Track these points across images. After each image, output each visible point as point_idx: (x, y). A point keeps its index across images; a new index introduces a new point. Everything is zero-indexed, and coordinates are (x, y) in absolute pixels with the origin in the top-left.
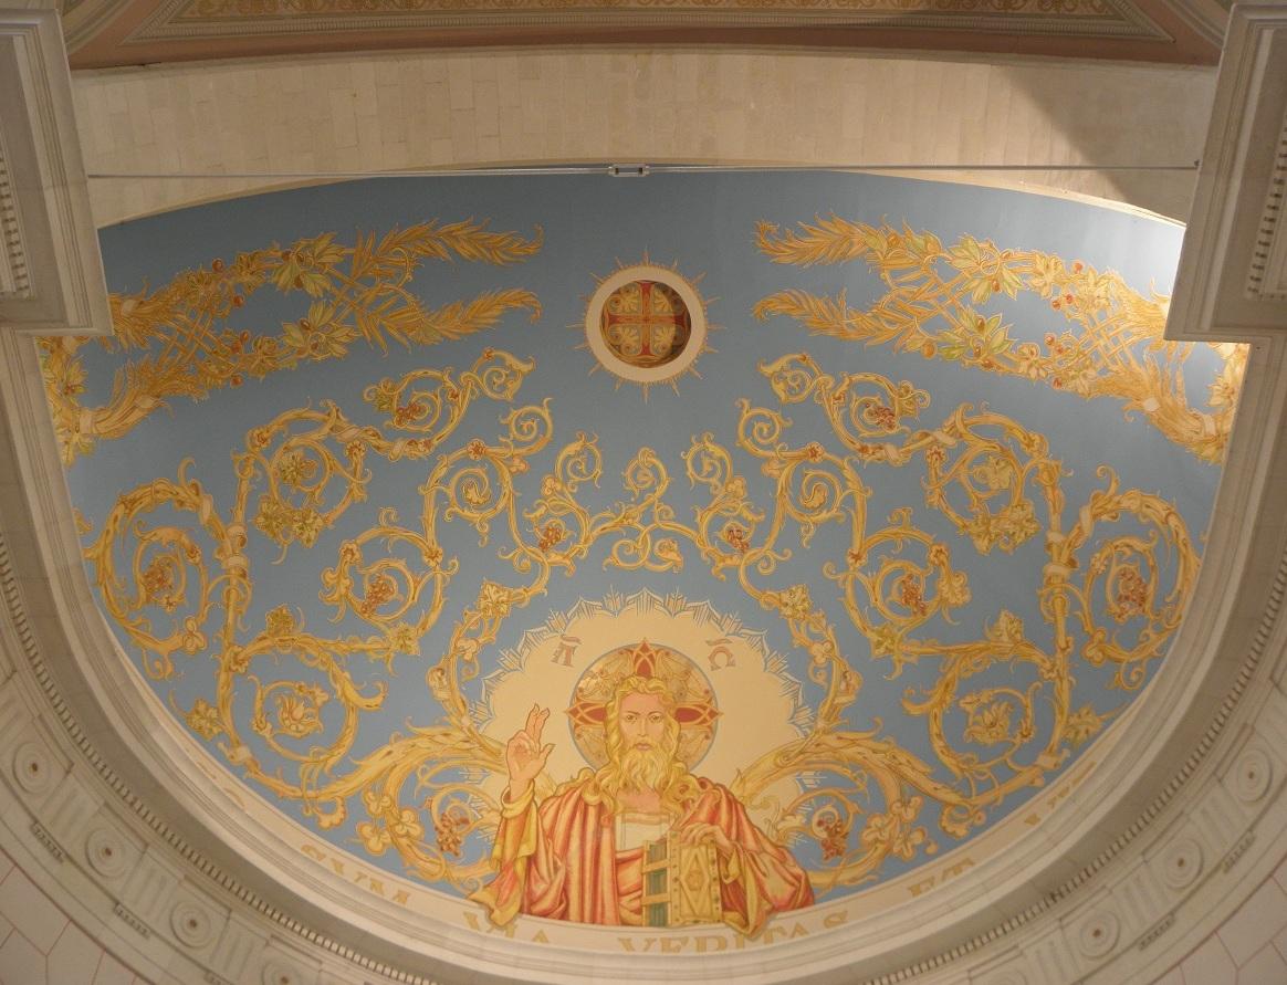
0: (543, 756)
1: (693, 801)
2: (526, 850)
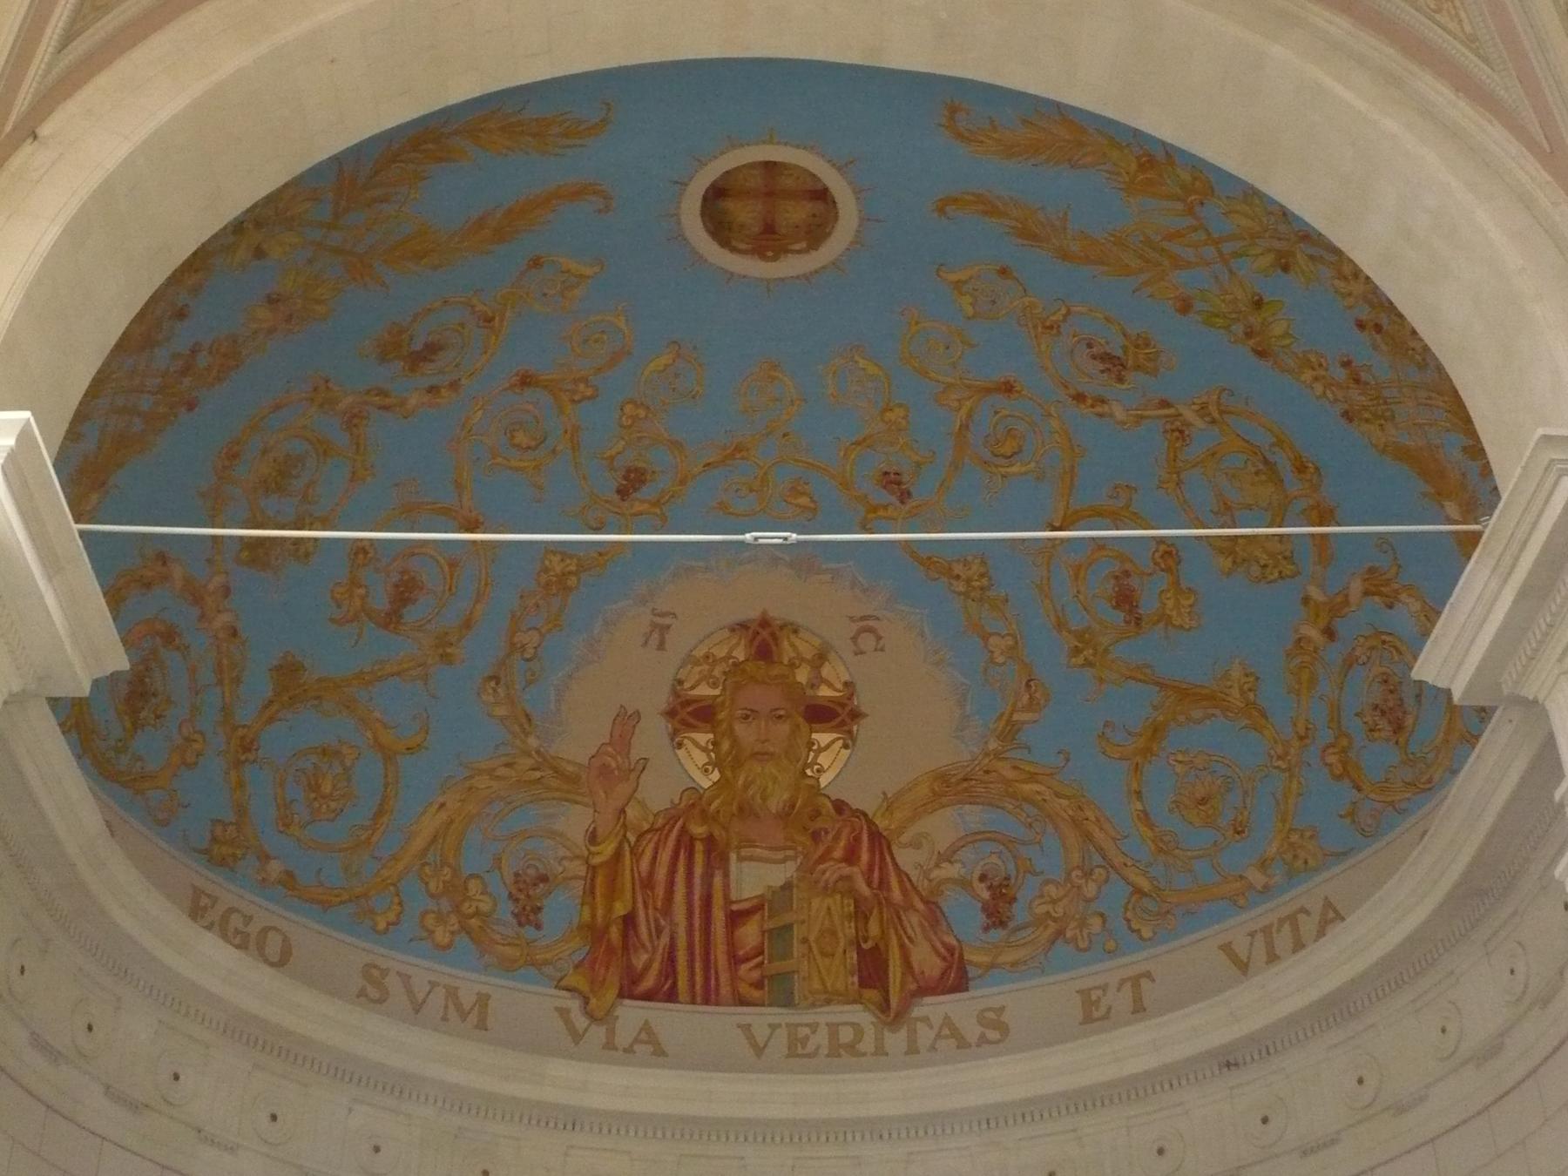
0: (633, 776)
1: (827, 833)
2: (620, 909)
